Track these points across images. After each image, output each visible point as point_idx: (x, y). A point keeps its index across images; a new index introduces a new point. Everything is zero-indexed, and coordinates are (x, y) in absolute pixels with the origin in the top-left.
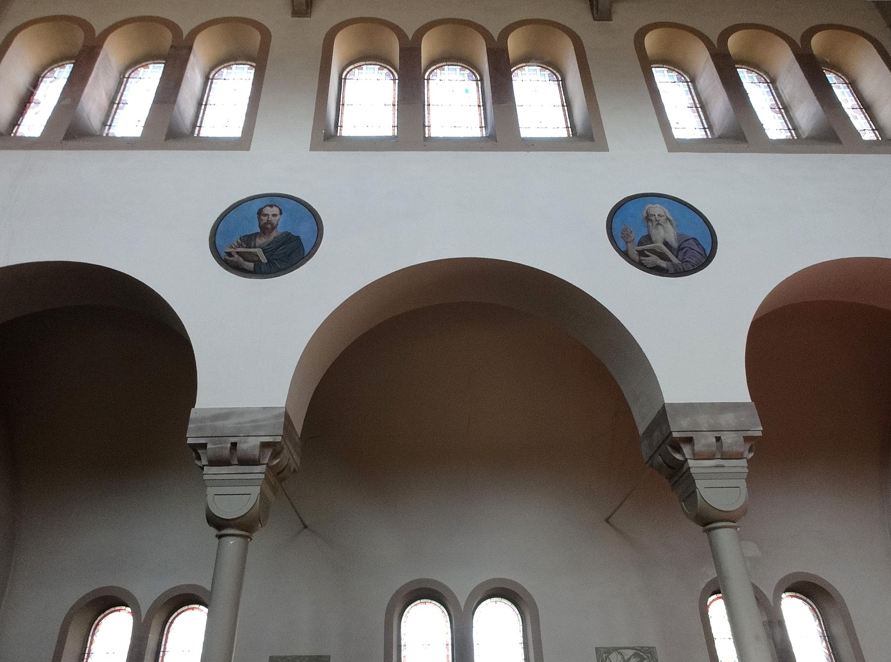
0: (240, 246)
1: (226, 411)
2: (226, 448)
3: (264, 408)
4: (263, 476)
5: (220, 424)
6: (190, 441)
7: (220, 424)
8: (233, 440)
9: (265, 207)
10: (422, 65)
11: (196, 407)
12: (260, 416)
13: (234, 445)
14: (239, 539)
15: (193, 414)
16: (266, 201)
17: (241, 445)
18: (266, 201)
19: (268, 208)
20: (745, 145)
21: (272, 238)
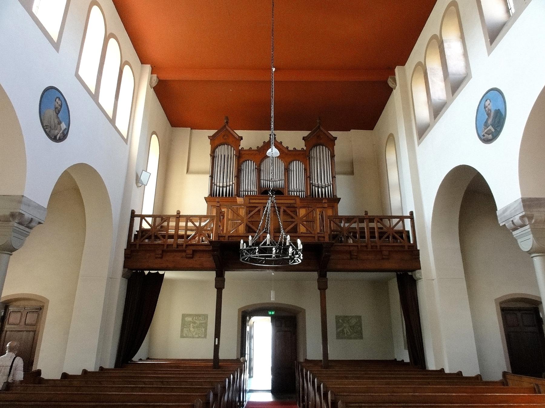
0: (485, 129)
1: (504, 209)
2: (510, 224)
3: (515, 201)
4: (530, 230)
5: (505, 214)
6: (501, 225)
7: (505, 214)
8: (511, 219)
9: (485, 103)
10: (404, 128)
11: (498, 210)
12: (515, 206)
13: (512, 221)
14: (538, 257)
15: (498, 213)
16: (483, 102)
17: (240, 232)
18: (483, 102)
19: (486, 102)
20: (418, 139)
21: (492, 118)
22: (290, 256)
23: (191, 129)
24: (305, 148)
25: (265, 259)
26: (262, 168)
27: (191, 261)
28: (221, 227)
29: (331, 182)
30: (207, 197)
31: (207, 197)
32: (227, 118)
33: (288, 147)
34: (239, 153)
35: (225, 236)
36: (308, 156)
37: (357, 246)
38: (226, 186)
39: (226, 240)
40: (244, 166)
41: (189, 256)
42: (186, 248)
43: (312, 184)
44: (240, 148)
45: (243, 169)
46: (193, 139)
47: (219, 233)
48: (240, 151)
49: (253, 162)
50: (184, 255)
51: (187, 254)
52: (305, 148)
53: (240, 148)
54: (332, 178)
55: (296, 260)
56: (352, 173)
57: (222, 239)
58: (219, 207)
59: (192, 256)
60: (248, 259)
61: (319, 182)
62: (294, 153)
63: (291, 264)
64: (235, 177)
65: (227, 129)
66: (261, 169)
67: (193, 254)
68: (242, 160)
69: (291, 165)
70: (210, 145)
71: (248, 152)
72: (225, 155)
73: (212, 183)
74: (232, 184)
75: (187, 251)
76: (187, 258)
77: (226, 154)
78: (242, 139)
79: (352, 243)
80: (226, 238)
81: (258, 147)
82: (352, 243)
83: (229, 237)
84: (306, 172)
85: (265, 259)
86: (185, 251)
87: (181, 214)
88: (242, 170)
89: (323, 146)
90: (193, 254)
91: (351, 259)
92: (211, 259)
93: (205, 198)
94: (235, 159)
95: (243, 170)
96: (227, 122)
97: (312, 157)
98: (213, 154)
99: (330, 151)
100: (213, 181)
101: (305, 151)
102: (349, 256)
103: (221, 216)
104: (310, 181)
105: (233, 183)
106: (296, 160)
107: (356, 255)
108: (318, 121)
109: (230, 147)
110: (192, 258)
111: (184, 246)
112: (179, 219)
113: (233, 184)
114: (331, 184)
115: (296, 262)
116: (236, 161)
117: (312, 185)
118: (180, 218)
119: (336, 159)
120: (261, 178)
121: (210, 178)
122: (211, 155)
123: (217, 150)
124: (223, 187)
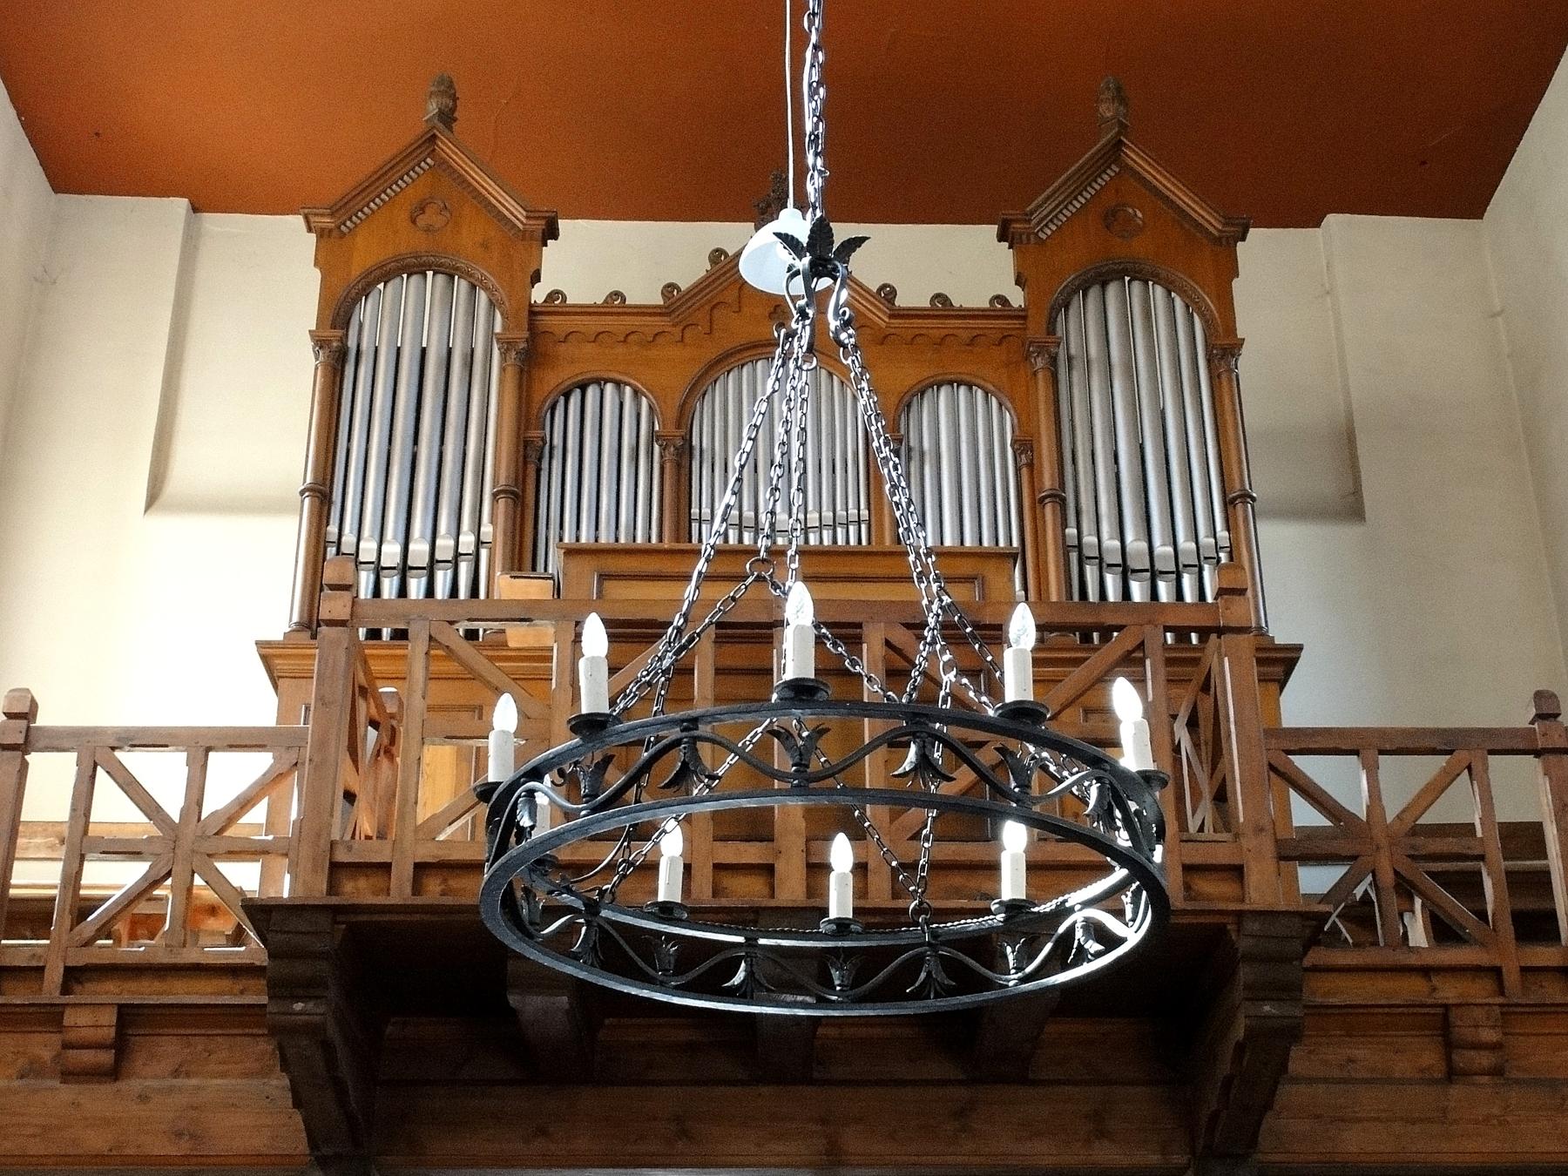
22: (1013, 908)
23: (196, 209)
24: (1017, 298)
25: (751, 942)
26: (705, 434)
27: (98, 1099)
28: (361, 802)
29: (1222, 533)
30: (281, 638)
31: (281, 638)
32: (448, 89)
33: (893, 292)
34: (532, 327)
35: (386, 867)
36: (1042, 348)
37: (1496, 972)
38: (424, 562)
39: (400, 891)
40: (565, 425)
41: (88, 1057)
42: (66, 990)
43: (1079, 547)
44: (538, 294)
45: (558, 441)
46: (205, 272)
47: (333, 844)
48: (533, 312)
49: (636, 393)
50: (47, 1055)
51: (67, 1046)
52: (1017, 298)
53: (538, 294)
54: (1228, 504)
55: (1079, 934)
56: (1352, 508)
57: (358, 891)
58: (342, 623)
59: (106, 1058)
60: (570, 930)
61: (1129, 537)
62: (934, 327)
63: (1023, 980)
64: (495, 496)
65: (443, 165)
66: (691, 447)
67: (121, 1045)
68: (551, 379)
69: (914, 408)
70: (317, 274)
71: (592, 324)
72: (424, 351)
73: (319, 546)
74: (471, 549)
75: (69, 1018)
76: (70, 1075)
77: (434, 337)
78: (555, 236)
79: (1424, 944)
80: (402, 875)
81: (670, 288)
82: (1424, 944)
83: (421, 868)
84: (1031, 465)
85: (751, 942)
86: (51, 1017)
87: (43, 720)
88: (552, 448)
89: (1144, 277)
90: (121, 1045)
91: (1452, 1074)
92: (279, 1083)
93: (269, 654)
94: (503, 370)
95: (558, 453)
96: (447, 117)
97: (1070, 359)
98: (339, 333)
99: (1202, 316)
100: (333, 529)
101: (1021, 315)
102: (1430, 1057)
103: (362, 718)
104: (1065, 525)
105: (479, 543)
106: (951, 383)
107: (1495, 1047)
108: (1107, 110)
109: (461, 286)
110: (114, 1073)
111: (54, 976)
112: (25, 766)
113: (484, 553)
114: (1218, 548)
115: (1082, 956)
116: (511, 385)
117: (1074, 556)
118: (33, 758)
119: (1247, 365)
120: (695, 510)
121: (307, 501)
122: (320, 343)
123: (366, 312)
124: (404, 570)
